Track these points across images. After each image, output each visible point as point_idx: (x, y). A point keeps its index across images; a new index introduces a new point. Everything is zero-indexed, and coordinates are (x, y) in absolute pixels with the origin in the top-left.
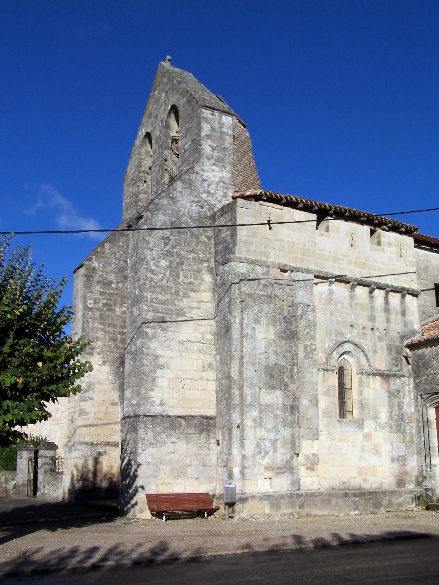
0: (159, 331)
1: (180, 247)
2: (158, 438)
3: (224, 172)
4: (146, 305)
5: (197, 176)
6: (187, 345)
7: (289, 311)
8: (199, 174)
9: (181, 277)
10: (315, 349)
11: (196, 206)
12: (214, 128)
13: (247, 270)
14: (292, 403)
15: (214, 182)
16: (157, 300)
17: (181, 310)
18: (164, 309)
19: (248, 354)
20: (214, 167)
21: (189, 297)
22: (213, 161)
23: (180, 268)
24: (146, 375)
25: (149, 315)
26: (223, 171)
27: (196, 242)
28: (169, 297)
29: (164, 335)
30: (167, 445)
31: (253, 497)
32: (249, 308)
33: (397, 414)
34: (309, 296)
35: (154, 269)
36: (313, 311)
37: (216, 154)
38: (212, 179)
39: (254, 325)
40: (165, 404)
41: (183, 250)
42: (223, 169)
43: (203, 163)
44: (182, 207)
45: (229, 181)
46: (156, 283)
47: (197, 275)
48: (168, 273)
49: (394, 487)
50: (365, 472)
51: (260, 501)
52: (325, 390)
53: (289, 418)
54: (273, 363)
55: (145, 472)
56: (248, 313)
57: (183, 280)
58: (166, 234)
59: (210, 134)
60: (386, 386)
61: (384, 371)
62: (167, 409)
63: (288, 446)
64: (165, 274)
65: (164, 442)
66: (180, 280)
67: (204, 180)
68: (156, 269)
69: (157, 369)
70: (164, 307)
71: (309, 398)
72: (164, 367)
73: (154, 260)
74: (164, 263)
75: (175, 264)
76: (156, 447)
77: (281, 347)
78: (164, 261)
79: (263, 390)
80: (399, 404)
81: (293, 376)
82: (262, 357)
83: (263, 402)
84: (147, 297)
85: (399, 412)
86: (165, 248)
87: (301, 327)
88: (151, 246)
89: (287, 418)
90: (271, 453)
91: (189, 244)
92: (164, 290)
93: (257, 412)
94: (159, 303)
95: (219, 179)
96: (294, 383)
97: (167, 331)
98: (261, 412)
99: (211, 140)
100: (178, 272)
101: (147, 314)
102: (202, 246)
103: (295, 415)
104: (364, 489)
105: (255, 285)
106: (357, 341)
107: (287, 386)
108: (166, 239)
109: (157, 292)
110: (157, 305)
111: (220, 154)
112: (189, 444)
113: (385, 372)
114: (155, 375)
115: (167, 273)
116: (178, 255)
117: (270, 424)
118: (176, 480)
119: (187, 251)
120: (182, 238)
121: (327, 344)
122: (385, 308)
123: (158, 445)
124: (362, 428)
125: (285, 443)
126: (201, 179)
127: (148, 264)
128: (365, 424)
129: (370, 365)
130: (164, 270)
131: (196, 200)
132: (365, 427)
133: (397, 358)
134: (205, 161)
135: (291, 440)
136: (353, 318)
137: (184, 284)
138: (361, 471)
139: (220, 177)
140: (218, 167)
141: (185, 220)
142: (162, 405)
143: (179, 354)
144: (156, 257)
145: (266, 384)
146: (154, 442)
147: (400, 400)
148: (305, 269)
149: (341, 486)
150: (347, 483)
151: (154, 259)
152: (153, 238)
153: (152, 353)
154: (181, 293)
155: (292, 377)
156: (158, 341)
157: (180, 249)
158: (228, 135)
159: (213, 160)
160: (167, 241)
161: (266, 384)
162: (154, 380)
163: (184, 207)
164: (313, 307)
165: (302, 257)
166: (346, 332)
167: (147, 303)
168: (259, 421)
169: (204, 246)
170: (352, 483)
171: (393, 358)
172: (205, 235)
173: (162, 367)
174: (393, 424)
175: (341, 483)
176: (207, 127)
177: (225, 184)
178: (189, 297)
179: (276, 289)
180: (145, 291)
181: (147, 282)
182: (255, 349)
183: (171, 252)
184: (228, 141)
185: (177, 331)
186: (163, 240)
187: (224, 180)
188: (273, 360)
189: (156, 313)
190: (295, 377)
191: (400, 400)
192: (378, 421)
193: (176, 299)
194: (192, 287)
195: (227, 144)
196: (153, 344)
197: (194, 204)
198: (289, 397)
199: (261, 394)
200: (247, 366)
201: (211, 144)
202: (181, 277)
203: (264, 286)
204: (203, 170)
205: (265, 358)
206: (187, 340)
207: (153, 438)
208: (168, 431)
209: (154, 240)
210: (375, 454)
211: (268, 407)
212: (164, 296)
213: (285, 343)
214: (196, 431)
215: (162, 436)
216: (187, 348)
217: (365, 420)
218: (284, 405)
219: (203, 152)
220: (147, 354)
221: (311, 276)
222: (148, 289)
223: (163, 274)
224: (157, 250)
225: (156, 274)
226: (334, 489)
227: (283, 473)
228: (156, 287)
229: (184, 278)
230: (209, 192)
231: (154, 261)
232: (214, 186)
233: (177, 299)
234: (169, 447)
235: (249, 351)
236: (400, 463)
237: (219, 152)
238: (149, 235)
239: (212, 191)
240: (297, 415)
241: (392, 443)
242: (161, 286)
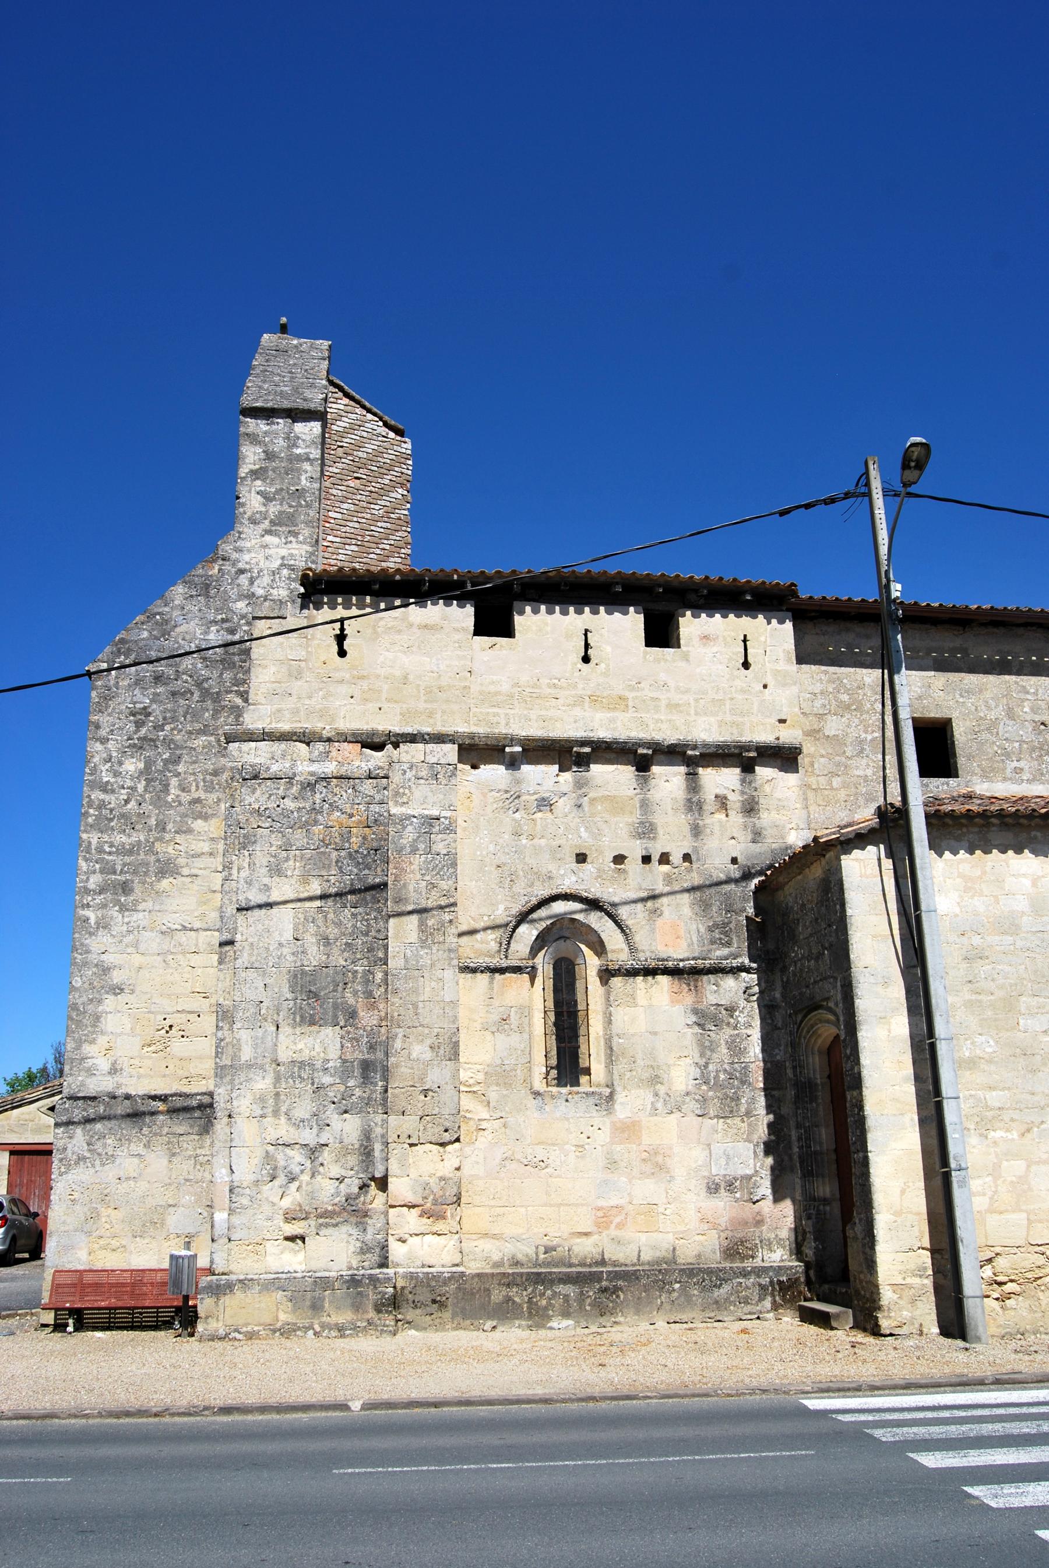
0: (114, 912)
1: (172, 726)
2: (98, 1146)
3: (294, 545)
4: (86, 860)
5: (223, 565)
6: (182, 937)
7: (364, 838)
8: (229, 560)
9: (174, 791)
10: (451, 921)
11: (218, 631)
12: (273, 451)
13: (269, 756)
14: (367, 1056)
15: (265, 572)
16: (111, 846)
17: (168, 861)
18: (129, 864)
19: (247, 948)
20: (268, 538)
21: (190, 831)
22: (266, 524)
23: (170, 771)
24: (78, 1010)
25: (91, 880)
26: (291, 542)
27: (213, 710)
28: (142, 838)
29: (126, 920)
30: (118, 1161)
31: (245, 1283)
32: (255, 842)
33: (727, 1067)
34: (441, 796)
35: (108, 782)
36: (450, 829)
37: (274, 509)
38: (261, 564)
39: (266, 880)
40: (121, 1069)
41: (180, 731)
42: (291, 539)
43: (240, 533)
44: (183, 639)
45: (306, 562)
46: (111, 810)
47: (212, 782)
48: (141, 787)
49: (714, 1259)
50: (618, 1220)
51: (265, 1292)
52: (495, 1017)
53: (358, 1092)
54: (315, 963)
55: (64, 1222)
56: (250, 855)
57: (178, 796)
58: (140, 703)
59: (261, 468)
60: (689, 999)
61: (681, 960)
62: (123, 1081)
63: (353, 1160)
64: (133, 789)
65: (112, 1156)
66: (169, 799)
67: (242, 572)
68: (112, 780)
69: (106, 996)
70: (127, 859)
71: (428, 1042)
72: (122, 990)
73: (110, 760)
74: (132, 766)
75: (160, 764)
76: (93, 1166)
77: (339, 924)
78: (134, 760)
79: (285, 1029)
80: (734, 1041)
81: (371, 991)
82: (286, 951)
83: (284, 1056)
84: (90, 843)
85: (732, 1063)
86: (136, 732)
87: (413, 872)
88: (103, 733)
89: (350, 1092)
90: (305, 1178)
91: (196, 716)
92: (129, 823)
93: (269, 1080)
94: (118, 853)
95: (279, 562)
96: (373, 1006)
97: (133, 910)
98: (278, 1079)
99: (264, 480)
100: (167, 780)
101: (88, 878)
102: (228, 716)
103: (376, 1085)
104: (615, 1264)
105: (279, 789)
106: (594, 891)
107: (352, 1015)
108: (140, 714)
109: (113, 829)
110: (111, 858)
111: (285, 507)
112: (174, 1159)
113: (681, 964)
114: (100, 1008)
115: (139, 786)
116: (168, 742)
117: (303, 1109)
118: (138, 1239)
119: (190, 733)
120: (179, 706)
121: (502, 907)
122: (689, 800)
123: (98, 1162)
124: (610, 1111)
125: (345, 1151)
126: (233, 570)
127: (94, 770)
128: (620, 1097)
129: (632, 949)
130: (132, 780)
131: (219, 617)
132: (617, 1106)
133: (725, 925)
134: (246, 530)
135: (361, 1145)
136: (584, 834)
137: (180, 804)
138: (604, 1218)
139: (283, 558)
140: (279, 536)
141: (190, 667)
142: (115, 1073)
143: (159, 958)
144: (114, 754)
145: (294, 1014)
146: (88, 1155)
147: (736, 1032)
148: (428, 735)
149: (542, 1256)
150: (558, 1249)
151: (109, 759)
152: (109, 715)
153: (95, 961)
154: (170, 826)
155: (369, 994)
156: (112, 935)
157: (172, 729)
158: (308, 459)
159: (267, 522)
160: (142, 717)
161: (294, 1014)
162: (97, 1018)
163: (188, 637)
164: (447, 822)
165: (429, 706)
166: (562, 872)
167: (88, 856)
168: (271, 1101)
169: (232, 716)
170: (576, 1249)
171: (716, 926)
172: (236, 691)
173: (117, 990)
174: (711, 1094)
175: (542, 1249)
176: (255, 453)
177: (293, 570)
178: (190, 831)
179: (337, 790)
180: (85, 831)
181: (91, 811)
182: (266, 935)
183: (151, 740)
184: (309, 474)
185: (157, 908)
186: (134, 715)
187: (292, 562)
188: (314, 956)
189: (108, 873)
190: (378, 993)
191: (736, 1032)
192: (662, 1089)
193: (157, 839)
194: (199, 809)
195: (305, 482)
196: (97, 943)
197: (212, 629)
198: (358, 1041)
199: (281, 1037)
200: (243, 975)
201: (263, 489)
202: (172, 791)
203: (303, 788)
204: (239, 550)
205: (293, 954)
206: (180, 927)
207: (86, 1147)
208: (122, 1129)
209: (111, 719)
210: (653, 1174)
211: (300, 1068)
212: (129, 836)
213: (353, 914)
214: (192, 1126)
215: (109, 1141)
216: (180, 945)
217: (618, 1089)
218: (345, 1061)
219: (241, 510)
220: (85, 964)
221: (450, 752)
222: (91, 826)
223: (128, 788)
224: (117, 740)
225: (113, 791)
226: (517, 1263)
227: (336, 1225)
228: (111, 820)
229: (179, 792)
230: (253, 594)
231: (109, 764)
232: (266, 580)
233: (160, 839)
234: (127, 1164)
235: (250, 940)
236: (738, 1195)
237: (281, 504)
238: (100, 711)
239: (260, 592)
240: (380, 1084)
241: (709, 1145)
242: (123, 816)
